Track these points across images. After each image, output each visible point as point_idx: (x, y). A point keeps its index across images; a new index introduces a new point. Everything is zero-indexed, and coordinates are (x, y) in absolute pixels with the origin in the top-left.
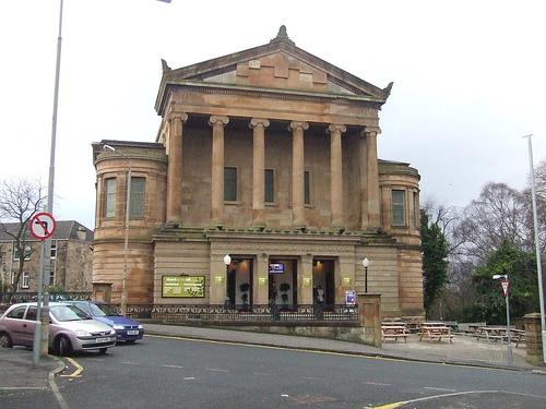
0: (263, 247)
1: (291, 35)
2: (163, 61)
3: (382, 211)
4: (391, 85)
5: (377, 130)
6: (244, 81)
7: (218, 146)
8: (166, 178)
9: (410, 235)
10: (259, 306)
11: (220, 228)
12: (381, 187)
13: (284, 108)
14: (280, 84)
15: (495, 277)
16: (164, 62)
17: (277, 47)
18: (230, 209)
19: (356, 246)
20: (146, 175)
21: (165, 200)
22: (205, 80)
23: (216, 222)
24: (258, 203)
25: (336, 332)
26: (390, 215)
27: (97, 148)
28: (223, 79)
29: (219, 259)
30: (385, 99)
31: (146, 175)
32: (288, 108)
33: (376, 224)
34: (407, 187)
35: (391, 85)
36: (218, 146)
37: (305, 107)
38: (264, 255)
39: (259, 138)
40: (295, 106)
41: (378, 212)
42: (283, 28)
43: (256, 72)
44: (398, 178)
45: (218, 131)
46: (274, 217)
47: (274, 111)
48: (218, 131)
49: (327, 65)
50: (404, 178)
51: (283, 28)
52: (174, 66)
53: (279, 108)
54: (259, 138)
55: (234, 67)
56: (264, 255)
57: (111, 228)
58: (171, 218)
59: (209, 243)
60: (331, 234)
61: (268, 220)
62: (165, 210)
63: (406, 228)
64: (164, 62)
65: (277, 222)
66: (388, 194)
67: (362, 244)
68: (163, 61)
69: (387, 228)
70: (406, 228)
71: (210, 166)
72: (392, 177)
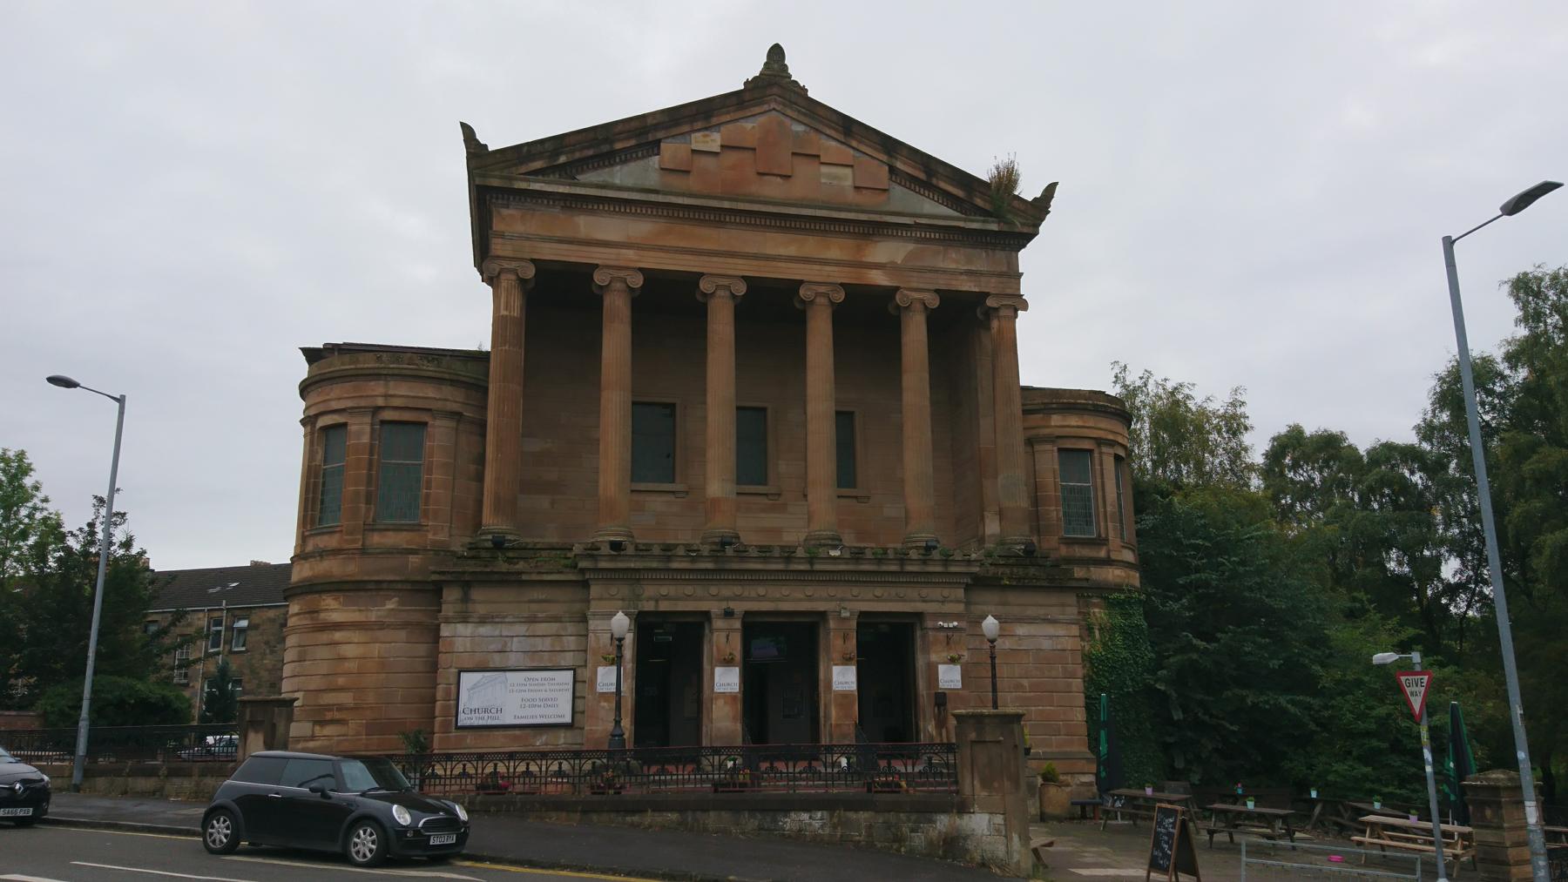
0: (726, 591)
1: (799, 70)
2: (463, 125)
3: (1036, 501)
4: (1051, 189)
5: (1020, 304)
6: (677, 182)
7: (616, 342)
8: (483, 425)
9: (1108, 562)
10: (716, 751)
11: (616, 546)
12: (1030, 442)
13: (783, 251)
14: (773, 189)
15: (1380, 657)
16: (468, 132)
17: (760, 101)
18: (656, 504)
19: (967, 588)
20: (424, 417)
21: (480, 478)
22: (582, 178)
23: (607, 533)
24: (718, 483)
25: (663, 768)
26: (1054, 512)
27: (124, 396)
28: (625, 176)
29: (316, 615)
30: (1037, 226)
31: (424, 417)
32: (792, 251)
33: (1019, 536)
34: (1100, 442)
35: (1051, 189)
36: (616, 342)
37: (836, 249)
38: (729, 614)
39: (721, 326)
40: (809, 245)
41: (1024, 502)
42: (776, 53)
43: (709, 162)
44: (1074, 421)
45: (617, 308)
46: (771, 520)
47: (755, 257)
48: (617, 308)
49: (890, 146)
50: (1091, 421)
51: (776, 53)
52: (495, 139)
53: (770, 251)
54: (721, 326)
55: (654, 147)
56: (729, 614)
57: (335, 552)
58: (489, 520)
59: (585, 584)
60: (903, 559)
61: (752, 527)
62: (479, 503)
63: (1101, 542)
64: (468, 132)
65: (777, 531)
66: (1049, 459)
67: (978, 584)
68: (463, 125)
69: (1052, 545)
70: (1101, 542)
71: (597, 385)
72: (1056, 420)
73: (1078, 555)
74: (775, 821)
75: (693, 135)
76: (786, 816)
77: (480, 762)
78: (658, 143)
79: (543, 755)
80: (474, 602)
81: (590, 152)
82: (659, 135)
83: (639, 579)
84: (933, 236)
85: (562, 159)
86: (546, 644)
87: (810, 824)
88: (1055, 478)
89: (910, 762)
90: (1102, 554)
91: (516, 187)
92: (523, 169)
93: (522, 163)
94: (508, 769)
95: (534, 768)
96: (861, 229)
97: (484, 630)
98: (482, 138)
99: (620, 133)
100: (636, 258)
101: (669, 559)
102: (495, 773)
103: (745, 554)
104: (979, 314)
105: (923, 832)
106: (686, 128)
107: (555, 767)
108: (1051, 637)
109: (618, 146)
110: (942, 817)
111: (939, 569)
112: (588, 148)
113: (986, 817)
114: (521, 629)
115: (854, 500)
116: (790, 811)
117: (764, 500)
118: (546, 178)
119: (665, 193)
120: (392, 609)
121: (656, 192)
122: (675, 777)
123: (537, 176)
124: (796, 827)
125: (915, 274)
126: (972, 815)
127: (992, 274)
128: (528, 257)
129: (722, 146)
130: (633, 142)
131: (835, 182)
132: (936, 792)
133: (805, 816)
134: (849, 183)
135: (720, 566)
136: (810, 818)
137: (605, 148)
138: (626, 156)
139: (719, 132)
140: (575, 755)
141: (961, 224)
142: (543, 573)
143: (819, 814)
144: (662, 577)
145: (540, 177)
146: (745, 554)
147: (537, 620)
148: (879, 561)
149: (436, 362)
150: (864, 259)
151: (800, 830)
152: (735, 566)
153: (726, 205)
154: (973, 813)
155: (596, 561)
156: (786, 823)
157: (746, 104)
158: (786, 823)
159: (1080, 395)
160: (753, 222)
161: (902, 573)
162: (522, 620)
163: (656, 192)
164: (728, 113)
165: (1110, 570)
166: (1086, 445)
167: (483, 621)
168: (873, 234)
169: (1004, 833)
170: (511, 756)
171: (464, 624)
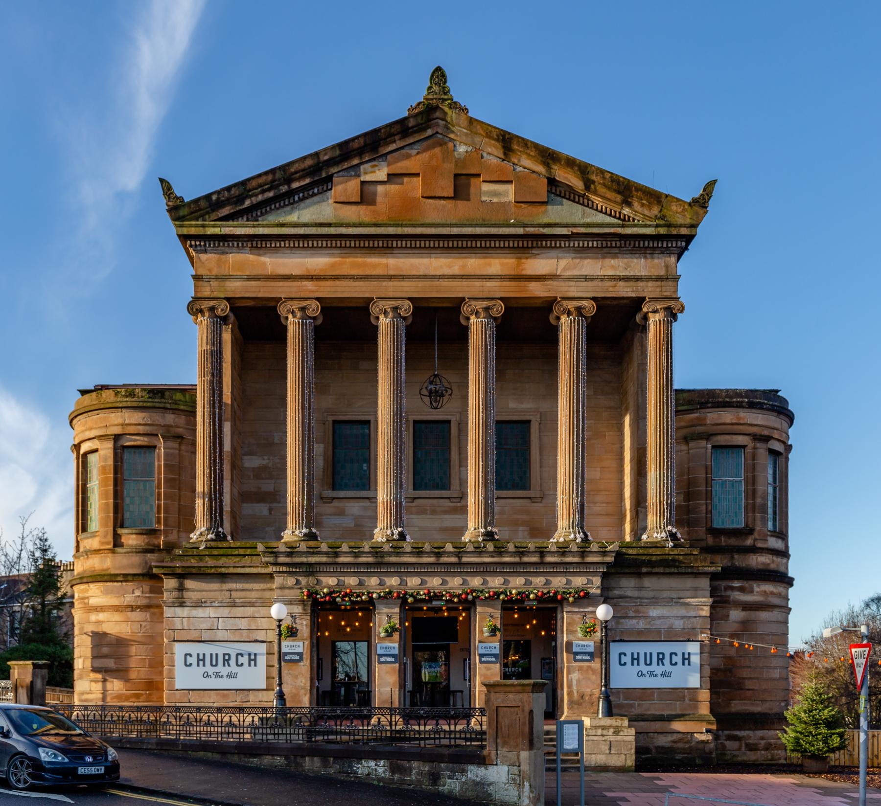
2: (162, 181)
9: (754, 550)
40: (473, 263)
55: (326, 183)
68: (162, 181)
73: (724, 544)
74: (351, 766)
75: (362, 167)
76: (358, 763)
77: (242, 715)
78: (329, 179)
79: (241, 710)
80: (187, 590)
81: (271, 194)
82: (333, 170)
83: (313, 572)
84: (590, 245)
85: (247, 203)
86: (243, 624)
87: (376, 770)
88: (706, 474)
89: (452, 722)
90: (749, 542)
91: (209, 233)
92: (214, 216)
93: (213, 211)
94: (239, 721)
95: (234, 719)
96: (385, 242)
97: (200, 612)
98: (178, 192)
99: (296, 173)
100: (314, 288)
101: (336, 554)
102: (425, 725)
103: (400, 550)
104: (638, 320)
105: (457, 779)
106: (356, 161)
107: (227, 719)
108: (682, 618)
109: (295, 185)
110: (472, 768)
111: (576, 559)
112: (269, 190)
113: (506, 768)
114: (225, 612)
115: (528, 501)
116: (361, 759)
117: (447, 503)
118: (235, 223)
119: (341, 225)
120: (139, 596)
121: (329, 225)
122: (220, 730)
123: (228, 221)
124: (366, 771)
125: (573, 283)
126: (495, 767)
127: (649, 279)
128: (223, 296)
129: (389, 175)
130: (308, 181)
131: (495, 200)
132: (471, 745)
133: (372, 763)
134: (511, 197)
135: (380, 560)
136: (376, 765)
137: (284, 189)
138: (306, 194)
139: (386, 160)
140: (263, 710)
141: (619, 230)
142: (238, 567)
143: (382, 762)
144: (328, 570)
145: (231, 223)
146: (400, 550)
147: (236, 604)
148: (563, 554)
149: (160, 395)
150: (524, 273)
151: (369, 774)
152: (393, 559)
153: (391, 231)
154: (496, 765)
155: (276, 557)
156: (358, 768)
157: (410, 131)
158: (358, 768)
159: (736, 393)
160: (273, 245)
161: (542, 563)
162: (225, 604)
163: (329, 225)
164: (394, 141)
165: (755, 557)
166: (740, 440)
167: (199, 604)
168: (532, 247)
169: (518, 782)
170: (219, 710)
171: (182, 608)
